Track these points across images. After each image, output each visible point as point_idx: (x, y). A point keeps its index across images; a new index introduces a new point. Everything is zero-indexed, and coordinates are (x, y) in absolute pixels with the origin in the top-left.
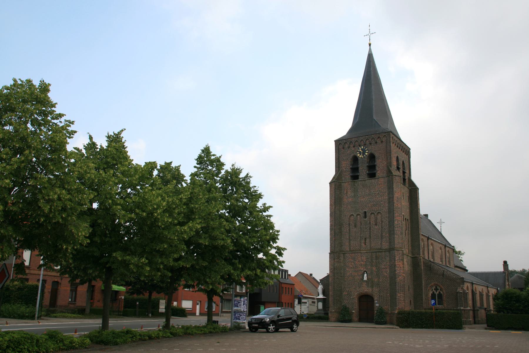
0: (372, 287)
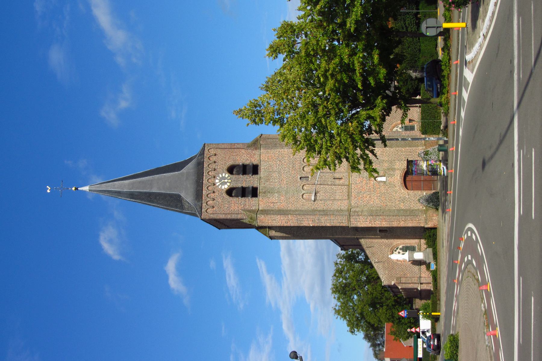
0: (394, 170)
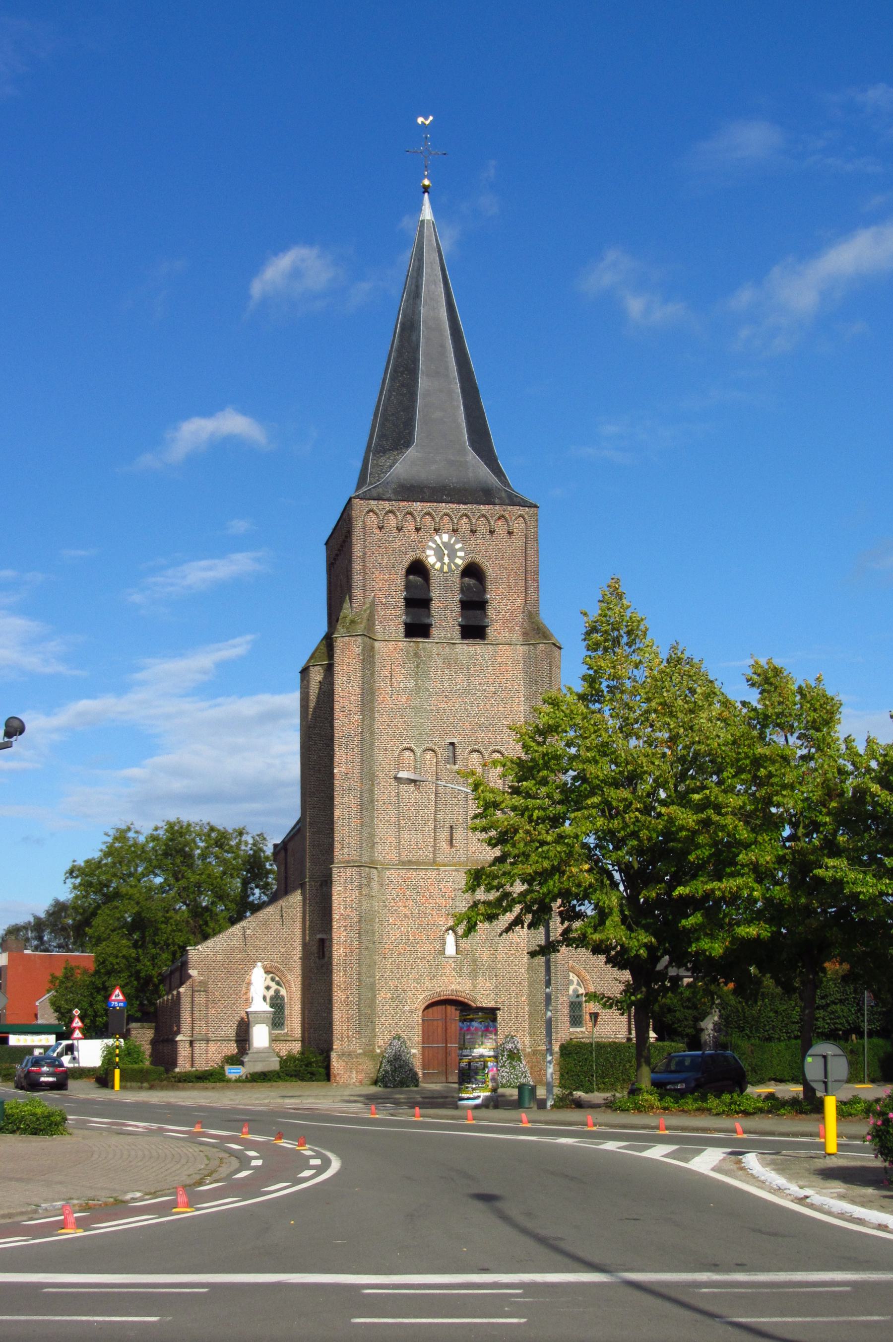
0: (473, 974)
